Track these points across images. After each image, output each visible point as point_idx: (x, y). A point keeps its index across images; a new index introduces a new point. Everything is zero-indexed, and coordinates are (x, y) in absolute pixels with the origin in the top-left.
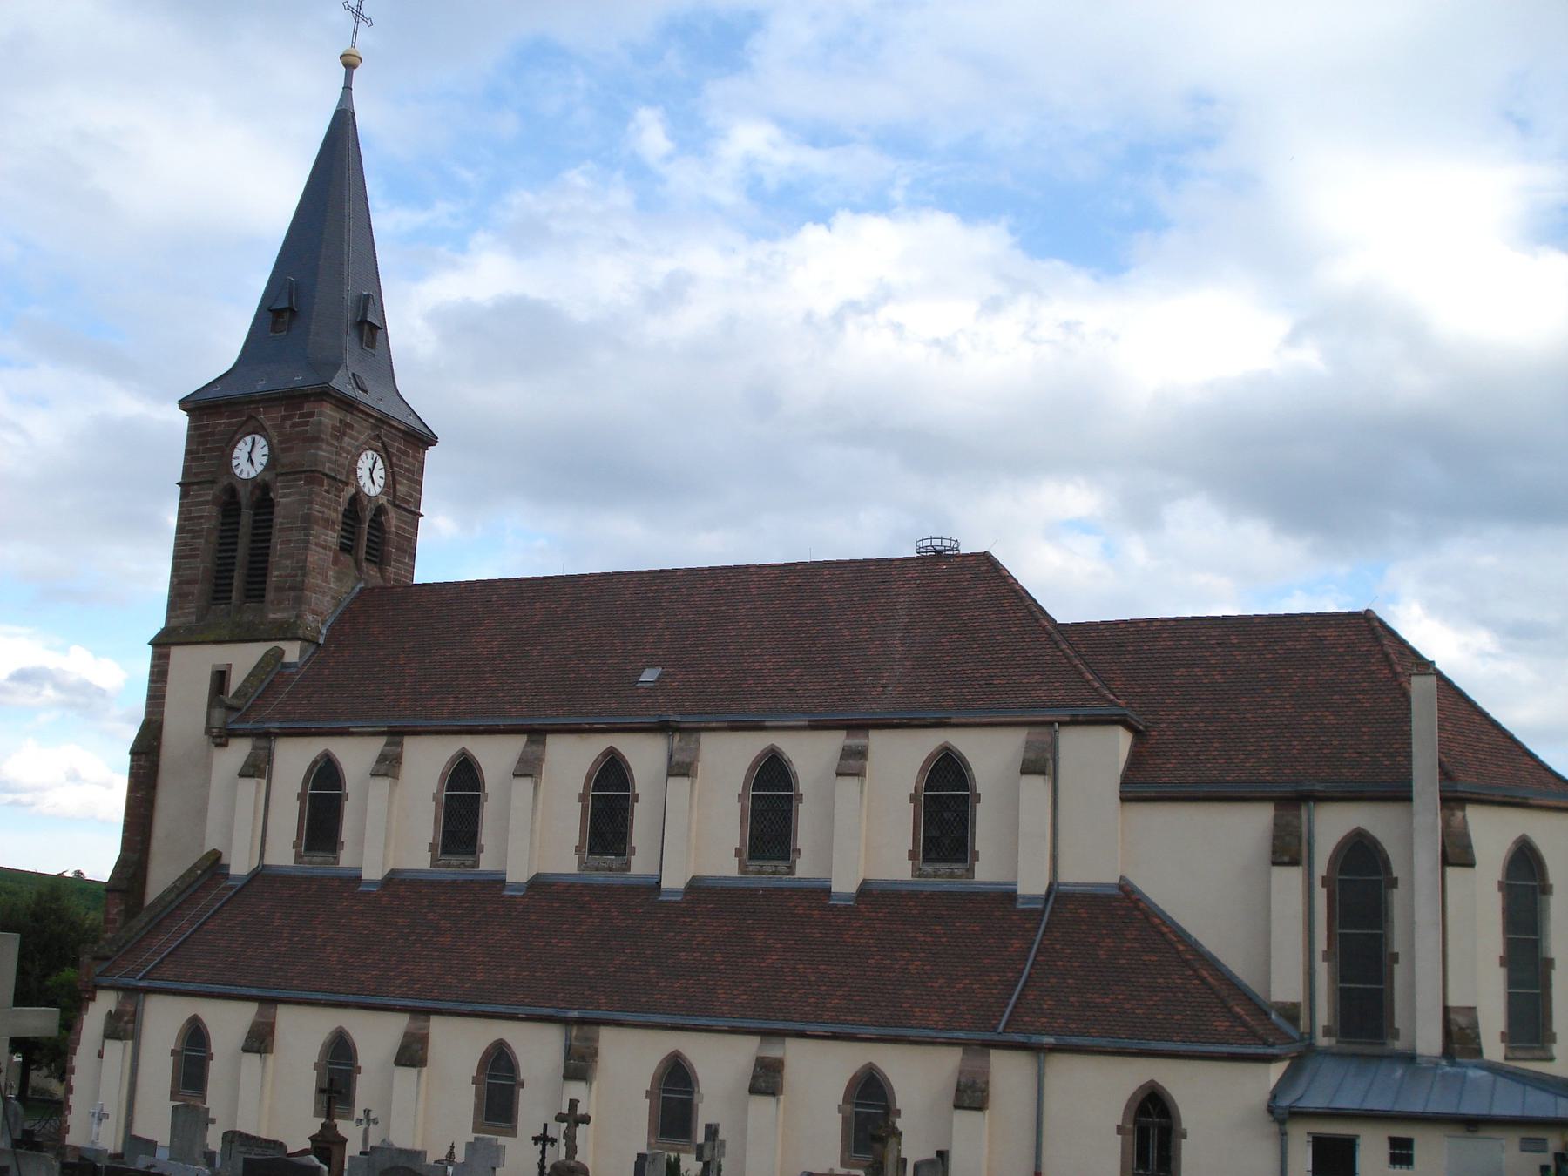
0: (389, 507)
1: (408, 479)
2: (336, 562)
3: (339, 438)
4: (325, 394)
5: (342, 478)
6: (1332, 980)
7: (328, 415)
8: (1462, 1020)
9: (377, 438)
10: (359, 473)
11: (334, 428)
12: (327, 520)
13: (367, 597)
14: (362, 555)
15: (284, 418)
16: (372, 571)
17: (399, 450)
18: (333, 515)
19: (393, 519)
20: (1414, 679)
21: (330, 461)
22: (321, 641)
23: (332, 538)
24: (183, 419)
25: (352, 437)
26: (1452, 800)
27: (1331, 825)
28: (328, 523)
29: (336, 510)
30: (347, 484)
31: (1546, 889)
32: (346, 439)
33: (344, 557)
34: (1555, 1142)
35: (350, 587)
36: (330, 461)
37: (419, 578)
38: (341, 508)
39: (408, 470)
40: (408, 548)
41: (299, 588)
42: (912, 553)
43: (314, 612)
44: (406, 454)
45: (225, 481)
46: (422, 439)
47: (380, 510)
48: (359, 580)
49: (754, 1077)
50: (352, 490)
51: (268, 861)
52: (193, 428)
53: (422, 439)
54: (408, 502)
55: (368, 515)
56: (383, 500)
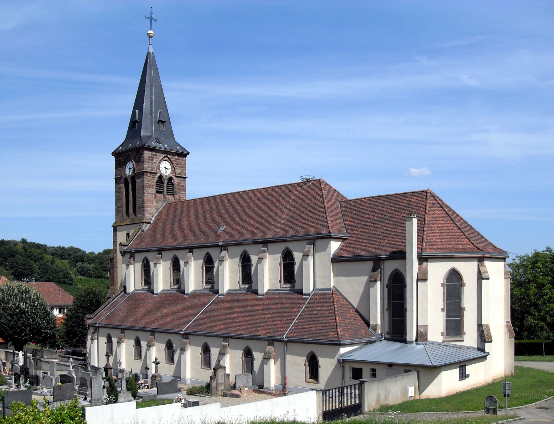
0: (174, 177)
1: (180, 167)
2: (155, 197)
3: (152, 160)
4: (143, 148)
5: (154, 172)
6: (389, 317)
7: (147, 154)
8: (422, 330)
9: (166, 156)
10: (161, 169)
11: (149, 157)
12: (150, 185)
13: (170, 207)
14: (165, 193)
15: (136, 156)
16: (171, 198)
17: (175, 159)
18: (153, 183)
19: (176, 181)
20: (407, 222)
21: (149, 167)
22: (152, 222)
23: (153, 191)
24: (113, 158)
25: (156, 158)
26: (422, 259)
27: (389, 267)
28: (151, 186)
29: (153, 182)
30: (156, 173)
31: (462, 285)
32: (154, 160)
33: (158, 195)
34: (158, 422)
35: (162, 205)
36: (149, 167)
37: (188, 198)
38: (156, 181)
39: (180, 164)
40: (183, 188)
41: (143, 207)
42: (299, 181)
43: (149, 214)
44: (179, 159)
45: (124, 177)
46: (183, 154)
47: (170, 179)
48: (165, 201)
49: (512, 290)
50: (159, 175)
51: (136, 288)
52: (117, 161)
53: (183, 154)
54: (181, 174)
55: (166, 182)
56: (171, 175)
